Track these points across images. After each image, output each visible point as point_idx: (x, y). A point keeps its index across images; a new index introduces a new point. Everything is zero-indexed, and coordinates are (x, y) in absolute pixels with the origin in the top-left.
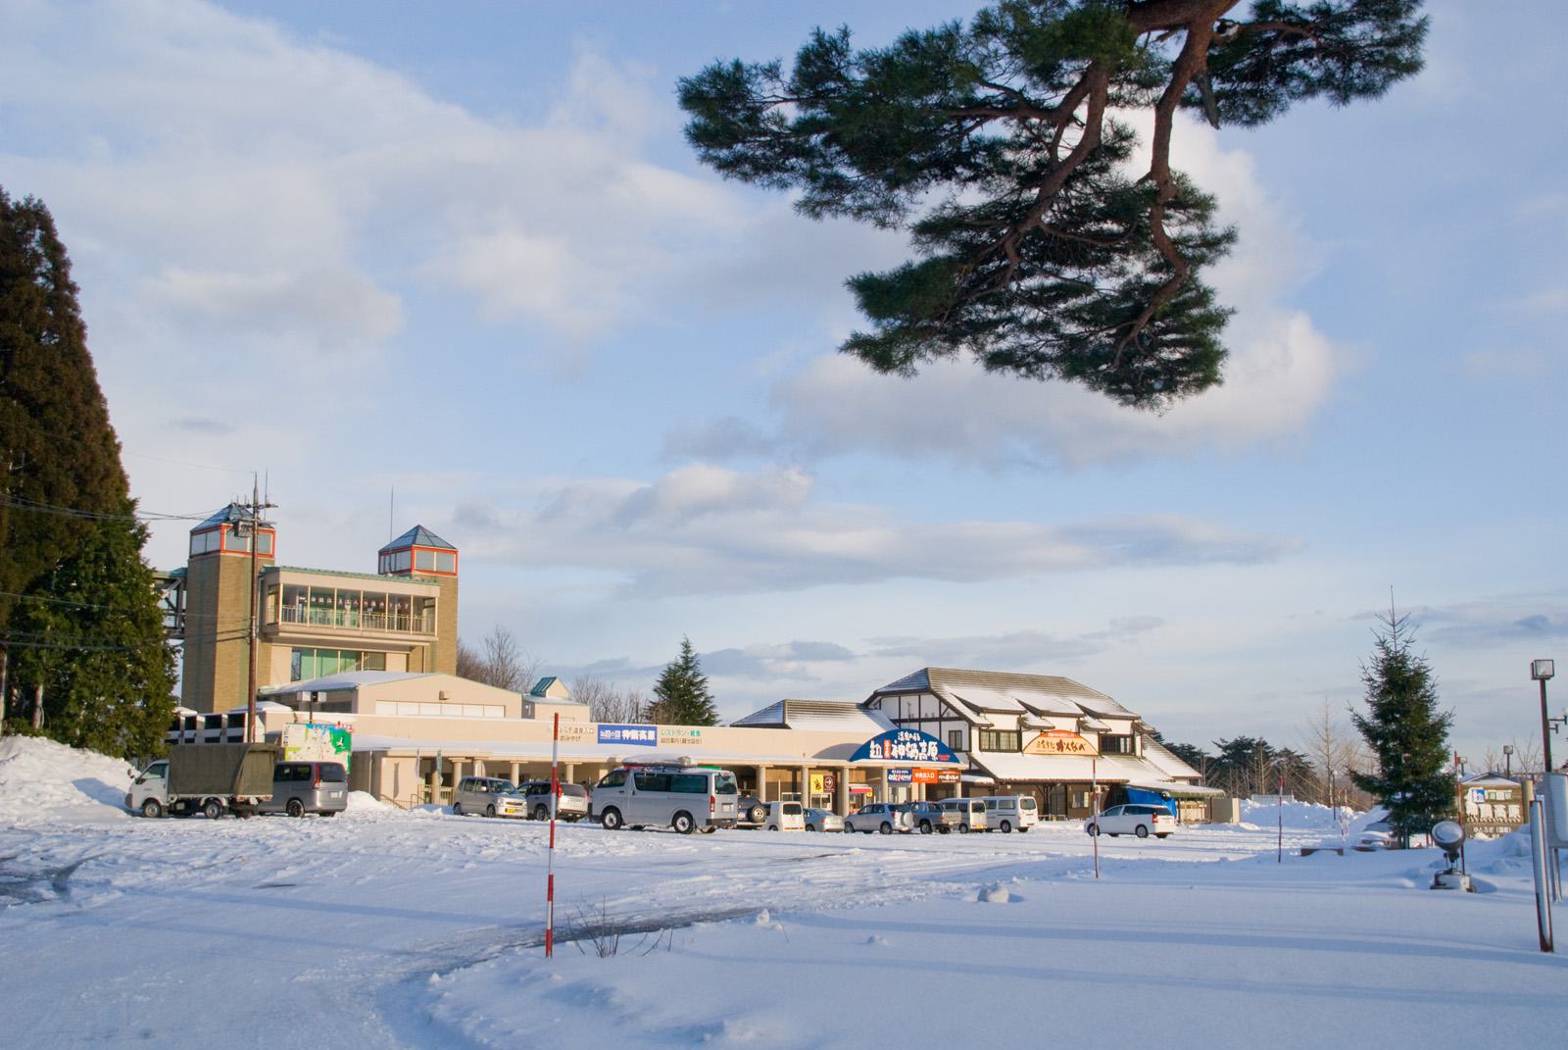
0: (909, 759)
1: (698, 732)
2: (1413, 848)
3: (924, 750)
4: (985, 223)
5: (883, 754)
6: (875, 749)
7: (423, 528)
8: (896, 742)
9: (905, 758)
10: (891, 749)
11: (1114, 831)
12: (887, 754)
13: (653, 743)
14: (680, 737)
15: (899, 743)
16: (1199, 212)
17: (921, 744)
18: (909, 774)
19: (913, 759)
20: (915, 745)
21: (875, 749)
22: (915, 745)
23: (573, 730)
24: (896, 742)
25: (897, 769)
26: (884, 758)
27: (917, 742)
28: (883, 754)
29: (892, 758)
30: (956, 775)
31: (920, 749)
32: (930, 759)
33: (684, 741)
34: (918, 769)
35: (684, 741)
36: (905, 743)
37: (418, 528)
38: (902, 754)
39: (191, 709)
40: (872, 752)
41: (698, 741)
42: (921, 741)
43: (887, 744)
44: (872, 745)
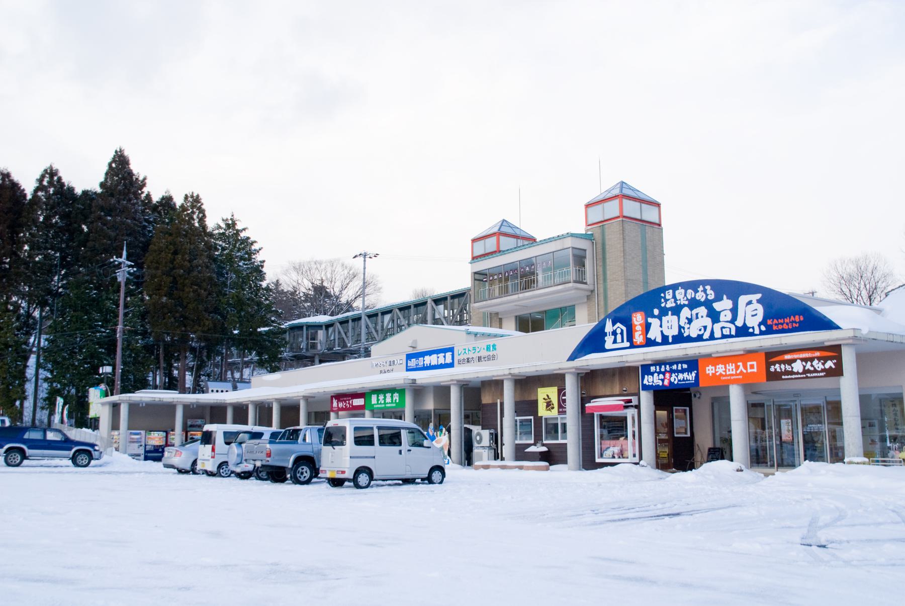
0: (689, 339)
1: (494, 346)
2: (164, 431)
3: (726, 316)
4: (64, 333)
5: (630, 338)
6: (614, 333)
7: (506, 221)
8: (656, 312)
9: (680, 338)
10: (647, 327)
11: (254, 459)
12: (638, 338)
13: (451, 365)
14: (476, 356)
15: (664, 312)
16: (222, 265)
17: (717, 306)
18: (689, 370)
19: (700, 338)
20: (703, 311)
21: (614, 333)
22: (703, 311)
23: (388, 363)
24: (656, 312)
25: (659, 363)
26: (633, 346)
27: (708, 304)
28: (630, 338)
29: (650, 343)
30: (825, 359)
31: (714, 316)
32: (744, 331)
33: (479, 359)
34: (712, 359)
35: (479, 359)
36: (677, 311)
37: (504, 221)
38: (672, 332)
39: (830, 352)
40: (609, 340)
41: (494, 356)
42: (718, 299)
43: (638, 319)
44: (609, 328)
